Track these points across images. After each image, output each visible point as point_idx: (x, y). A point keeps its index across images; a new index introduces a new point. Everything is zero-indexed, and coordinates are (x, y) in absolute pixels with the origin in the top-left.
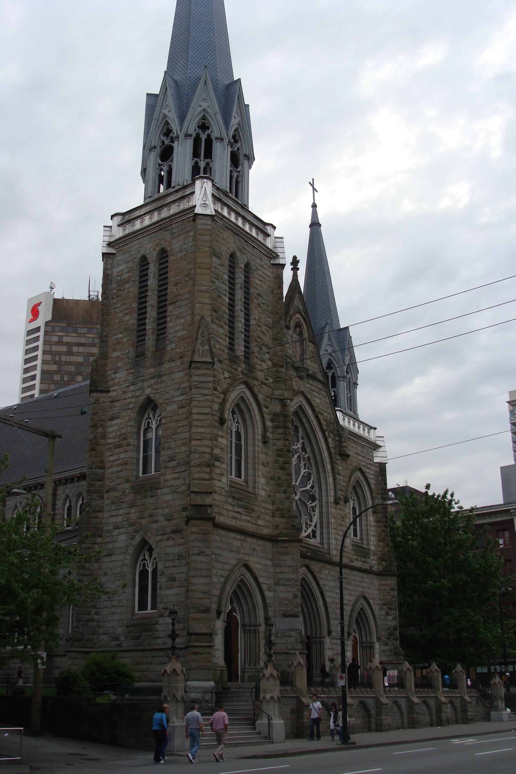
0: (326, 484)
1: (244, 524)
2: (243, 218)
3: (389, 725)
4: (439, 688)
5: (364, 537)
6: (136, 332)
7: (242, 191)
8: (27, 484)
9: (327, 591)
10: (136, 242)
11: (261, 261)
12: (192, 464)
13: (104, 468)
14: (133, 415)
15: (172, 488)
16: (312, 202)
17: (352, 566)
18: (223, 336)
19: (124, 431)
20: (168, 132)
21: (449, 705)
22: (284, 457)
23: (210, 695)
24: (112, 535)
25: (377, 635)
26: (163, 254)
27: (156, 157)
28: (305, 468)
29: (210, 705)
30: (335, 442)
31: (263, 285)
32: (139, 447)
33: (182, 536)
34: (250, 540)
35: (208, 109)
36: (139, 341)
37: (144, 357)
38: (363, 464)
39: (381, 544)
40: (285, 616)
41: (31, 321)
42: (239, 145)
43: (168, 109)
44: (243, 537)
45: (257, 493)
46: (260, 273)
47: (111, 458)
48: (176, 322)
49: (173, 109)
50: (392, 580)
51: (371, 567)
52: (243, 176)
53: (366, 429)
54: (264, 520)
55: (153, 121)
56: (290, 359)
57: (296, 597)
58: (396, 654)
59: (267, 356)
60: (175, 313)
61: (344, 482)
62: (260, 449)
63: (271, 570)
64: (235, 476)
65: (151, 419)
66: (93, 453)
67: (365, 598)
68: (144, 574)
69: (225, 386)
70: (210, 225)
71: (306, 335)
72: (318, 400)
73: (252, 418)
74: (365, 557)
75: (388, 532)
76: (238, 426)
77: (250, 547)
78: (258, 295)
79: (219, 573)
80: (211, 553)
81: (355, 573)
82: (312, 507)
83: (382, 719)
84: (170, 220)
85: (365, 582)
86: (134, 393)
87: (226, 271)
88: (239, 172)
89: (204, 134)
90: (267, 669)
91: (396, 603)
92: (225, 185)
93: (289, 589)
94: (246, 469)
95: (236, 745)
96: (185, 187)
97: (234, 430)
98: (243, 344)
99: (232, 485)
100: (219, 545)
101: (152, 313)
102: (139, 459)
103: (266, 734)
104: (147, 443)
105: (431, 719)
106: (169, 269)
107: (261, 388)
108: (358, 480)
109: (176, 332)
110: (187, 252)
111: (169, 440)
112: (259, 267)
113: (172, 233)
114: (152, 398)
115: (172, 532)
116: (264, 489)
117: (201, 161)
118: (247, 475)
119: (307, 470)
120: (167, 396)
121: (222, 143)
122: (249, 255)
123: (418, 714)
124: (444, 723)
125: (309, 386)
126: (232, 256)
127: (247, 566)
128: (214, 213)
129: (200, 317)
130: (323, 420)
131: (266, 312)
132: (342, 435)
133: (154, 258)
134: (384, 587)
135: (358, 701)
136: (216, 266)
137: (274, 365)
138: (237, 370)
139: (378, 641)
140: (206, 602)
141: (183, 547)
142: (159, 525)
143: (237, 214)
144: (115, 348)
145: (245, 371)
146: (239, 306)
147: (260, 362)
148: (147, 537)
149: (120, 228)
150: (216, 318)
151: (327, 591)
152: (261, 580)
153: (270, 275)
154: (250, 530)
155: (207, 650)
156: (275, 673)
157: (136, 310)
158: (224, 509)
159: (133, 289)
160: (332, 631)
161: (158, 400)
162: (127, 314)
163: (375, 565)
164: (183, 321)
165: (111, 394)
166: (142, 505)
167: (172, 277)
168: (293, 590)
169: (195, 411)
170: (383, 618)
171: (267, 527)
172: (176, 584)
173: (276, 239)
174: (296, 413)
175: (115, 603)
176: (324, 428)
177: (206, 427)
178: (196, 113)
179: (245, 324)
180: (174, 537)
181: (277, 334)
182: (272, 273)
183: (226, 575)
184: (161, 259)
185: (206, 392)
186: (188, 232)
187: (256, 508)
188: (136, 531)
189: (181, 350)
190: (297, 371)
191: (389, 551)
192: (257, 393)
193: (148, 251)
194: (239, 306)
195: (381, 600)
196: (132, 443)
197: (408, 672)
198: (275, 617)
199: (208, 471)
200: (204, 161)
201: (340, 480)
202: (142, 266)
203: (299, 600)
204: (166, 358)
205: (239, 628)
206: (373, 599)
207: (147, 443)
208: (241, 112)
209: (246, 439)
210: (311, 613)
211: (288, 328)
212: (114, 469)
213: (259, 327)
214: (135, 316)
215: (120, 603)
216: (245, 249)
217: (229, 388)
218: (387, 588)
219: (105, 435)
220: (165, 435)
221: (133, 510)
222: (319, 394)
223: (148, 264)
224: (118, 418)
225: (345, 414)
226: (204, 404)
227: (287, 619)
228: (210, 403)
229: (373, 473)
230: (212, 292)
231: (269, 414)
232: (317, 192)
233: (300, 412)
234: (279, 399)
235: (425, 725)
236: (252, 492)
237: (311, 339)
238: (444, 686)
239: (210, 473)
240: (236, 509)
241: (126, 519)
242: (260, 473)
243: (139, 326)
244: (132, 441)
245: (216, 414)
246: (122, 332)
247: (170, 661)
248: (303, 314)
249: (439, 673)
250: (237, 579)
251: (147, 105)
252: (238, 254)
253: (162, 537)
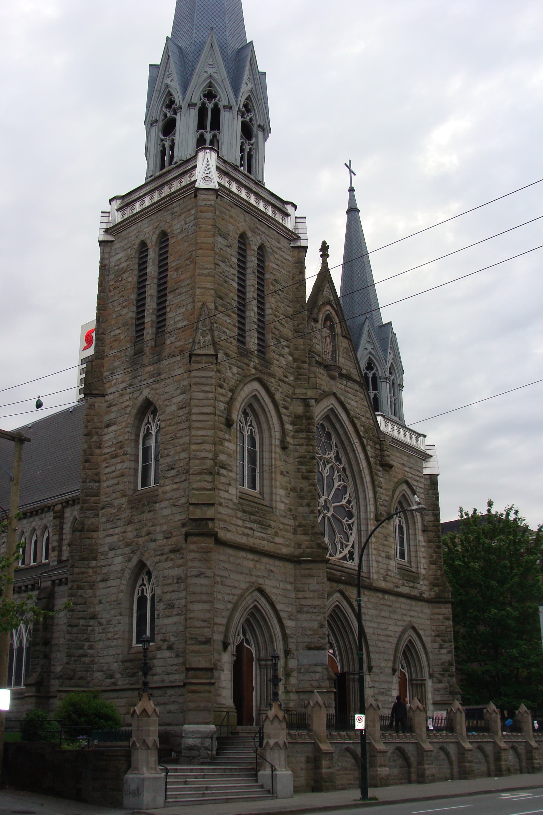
0: (365, 498)
1: (257, 542)
2: (256, 194)
3: (433, 775)
4: (497, 732)
5: (413, 559)
6: (134, 326)
7: (256, 165)
8: (33, 507)
9: (367, 621)
10: (135, 226)
11: (279, 243)
12: (191, 471)
13: (99, 482)
14: (131, 420)
15: (171, 501)
16: (349, 186)
17: (398, 592)
18: (230, 326)
19: (120, 439)
20: (170, 104)
21: (511, 752)
22: (307, 465)
23: (210, 740)
24: (107, 557)
25: (429, 672)
26: (164, 237)
27: (158, 131)
28: (339, 481)
29: (210, 752)
30: (375, 451)
31: (282, 270)
32: (138, 456)
33: (181, 556)
34: (265, 560)
35: (215, 75)
36: (137, 337)
37: (143, 354)
38: (410, 475)
39: (433, 567)
40: (309, 648)
41: (85, 349)
42: (252, 114)
44: (256, 557)
45: (274, 506)
46: (277, 256)
47: (107, 470)
48: (177, 312)
49: (176, 78)
50: (446, 608)
51: (421, 594)
52: (256, 149)
53: (414, 436)
54: (283, 537)
55: (155, 92)
56: (319, 356)
57: (321, 626)
58: (452, 693)
59: (287, 350)
60: (176, 301)
61: (387, 496)
62: (277, 456)
63: (293, 595)
64: (248, 487)
65: (150, 423)
66: (87, 464)
67: (413, 628)
68: (142, 600)
69: (233, 383)
70: (213, 200)
71: (338, 330)
72: (353, 403)
73: (267, 421)
74: (413, 582)
75: (440, 553)
76: (251, 430)
77: (266, 568)
78: (275, 280)
79: (226, 599)
80: (212, 575)
81: (402, 600)
82: (349, 525)
83: (424, 769)
84: (171, 199)
85: (414, 611)
86: (131, 395)
87: (235, 253)
88: (252, 145)
89: (210, 103)
90: (271, 709)
91: (451, 634)
92: (234, 156)
93: (314, 617)
94: (262, 479)
95: (227, 801)
96: (188, 161)
97: (247, 435)
98: (256, 335)
99: (243, 497)
100: (226, 566)
101: (151, 304)
102: (138, 470)
103: (270, 787)
104: (146, 451)
105: (489, 769)
106: (169, 255)
107: (279, 386)
108: (404, 494)
109: (176, 323)
110: (188, 233)
111: (168, 447)
112: (276, 250)
113: (172, 213)
114: (151, 399)
115: (172, 551)
116: (283, 502)
117: (207, 132)
118: (262, 486)
119: (342, 482)
120: (166, 396)
121: (231, 111)
122: (263, 236)
123: (471, 762)
124: (504, 773)
125: (343, 386)
126: (243, 237)
127: (261, 591)
128: (217, 187)
129: (202, 303)
130: (361, 425)
131: (285, 300)
132: (384, 443)
133: (154, 243)
134: (437, 616)
135: (394, 748)
136: (222, 247)
137: (295, 360)
138: (248, 365)
139: (430, 678)
140: (207, 632)
141: (183, 568)
142: (157, 544)
143: (249, 190)
144: (112, 346)
145: (258, 366)
146: (251, 293)
147: (277, 356)
148: (144, 559)
149: (119, 213)
150: (222, 306)
151: (367, 621)
152: (279, 607)
153: (290, 259)
154: (266, 548)
155: (207, 688)
156: (281, 714)
157: (135, 302)
158: (233, 524)
159: (131, 279)
160: (372, 667)
161: (157, 401)
162: (124, 307)
163: (425, 591)
164: (183, 310)
165: (108, 398)
166: (139, 522)
167: (173, 262)
168: (319, 618)
169: (194, 410)
170: (436, 651)
171: (288, 546)
172: (175, 611)
173: (297, 219)
174: (327, 418)
175: (110, 635)
176: (362, 434)
177: (208, 428)
178: (201, 80)
179: (259, 314)
180: (173, 557)
181: (298, 325)
182: (293, 257)
183: (234, 601)
184: (161, 243)
185: (207, 388)
186: (189, 210)
187: (273, 524)
188: (133, 552)
189: (181, 343)
190: (327, 370)
191: (442, 575)
192: (275, 392)
193: (147, 235)
194: (252, 293)
195: (434, 631)
196: (129, 452)
197: (458, 713)
198: (297, 650)
199: (210, 480)
200: (210, 133)
201: (382, 493)
202: (141, 253)
203: (326, 630)
204: (166, 354)
205: (407, 683)
206: (424, 630)
207: (146, 451)
208: (254, 79)
209: (262, 445)
210: (348, 647)
211: (316, 321)
212: (111, 482)
213: (276, 317)
214: (134, 308)
215: (116, 635)
216: (258, 229)
217: (238, 385)
218: (441, 617)
219: (101, 444)
220: (164, 440)
221: (129, 528)
222: (356, 396)
223: (147, 250)
224: (114, 424)
225: (387, 419)
226: (206, 402)
227: (311, 652)
228: (213, 401)
229: (422, 486)
230: (216, 276)
231: (289, 416)
232: (355, 175)
233: (332, 417)
234: (301, 398)
235: (481, 775)
236: (268, 505)
237: (344, 334)
238: (503, 730)
239: (212, 482)
240: (248, 524)
241: (122, 539)
242: (278, 483)
243: (138, 319)
244: (129, 450)
245: (222, 415)
246: (120, 328)
247: (140, 700)
248: (335, 306)
249: (497, 714)
250: (249, 606)
252: (249, 234)
253: (160, 557)
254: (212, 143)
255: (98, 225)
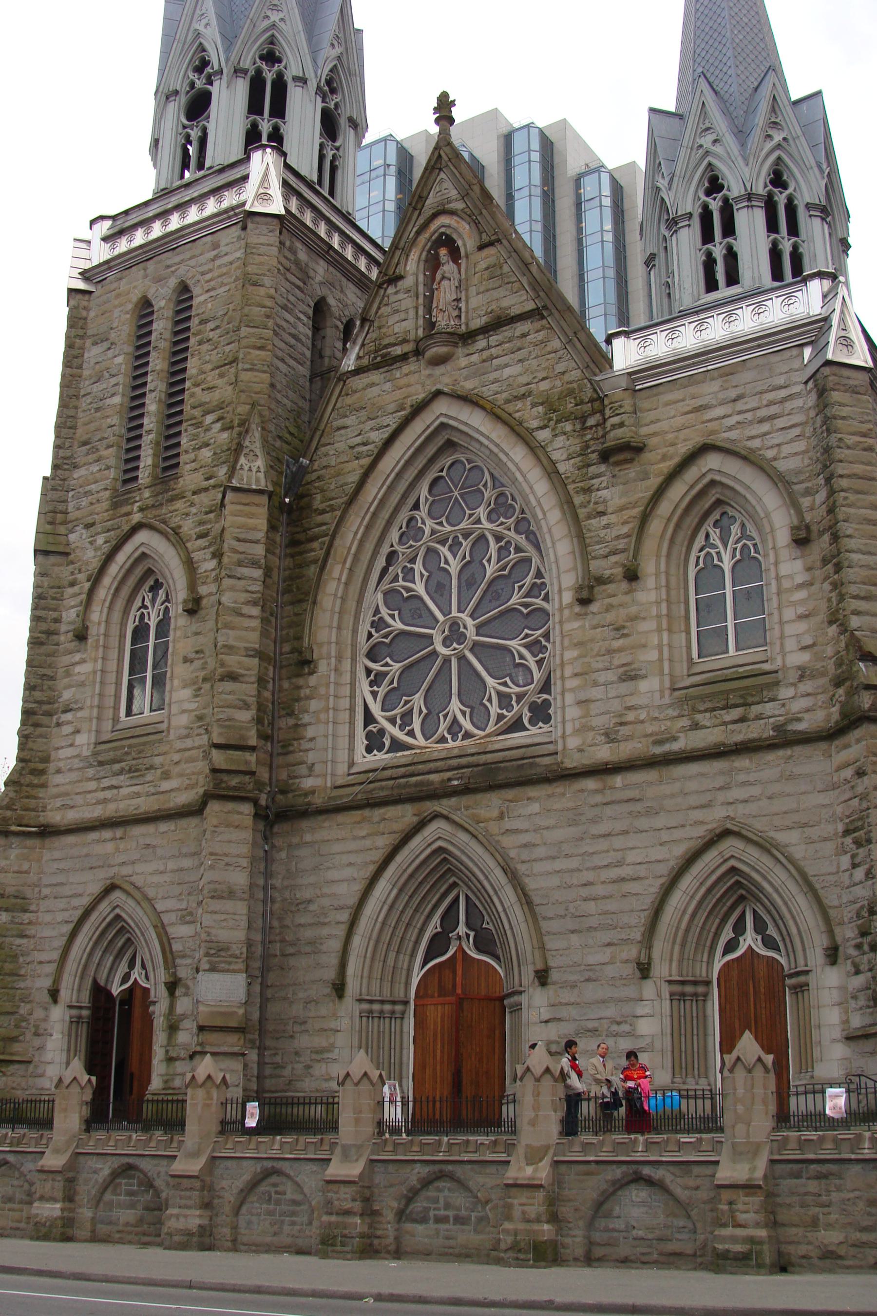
1: (122, 805)
20: (201, 66)
42: (337, 98)
43: (204, 22)
49: (214, 22)
65: (146, 607)
88: (338, 149)
92: (308, 168)
128: (283, 212)
251: (166, 19)
254: (270, 138)
255: (69, 261)
